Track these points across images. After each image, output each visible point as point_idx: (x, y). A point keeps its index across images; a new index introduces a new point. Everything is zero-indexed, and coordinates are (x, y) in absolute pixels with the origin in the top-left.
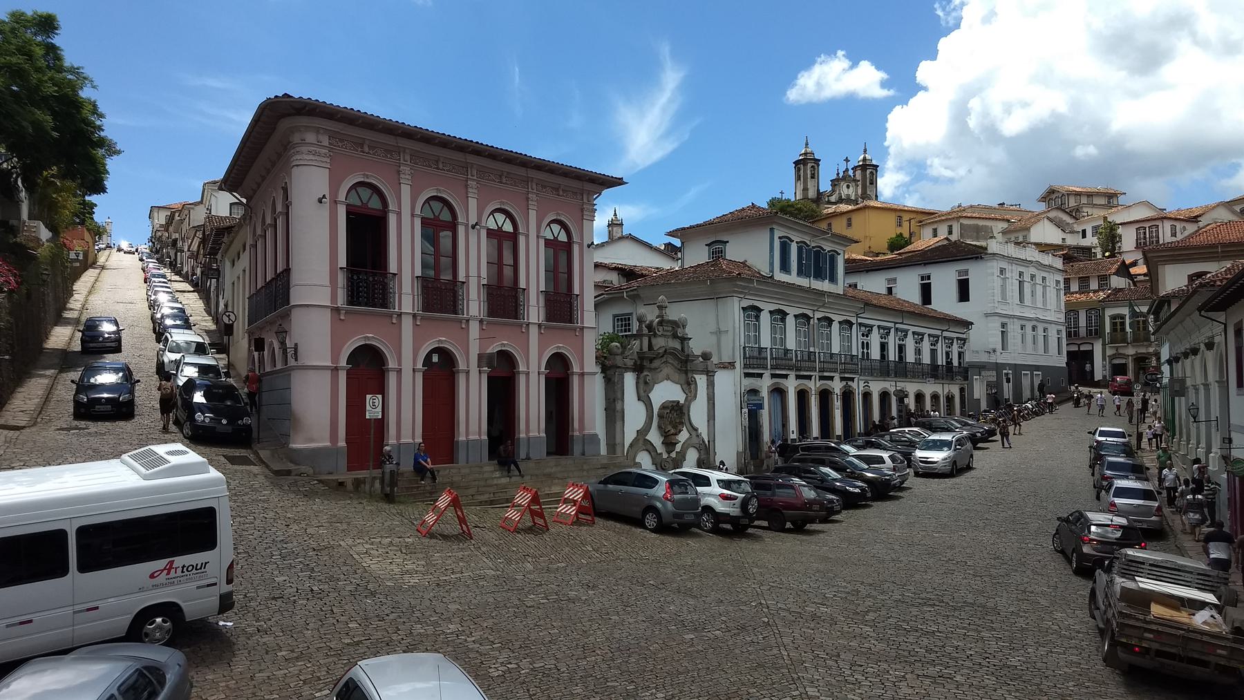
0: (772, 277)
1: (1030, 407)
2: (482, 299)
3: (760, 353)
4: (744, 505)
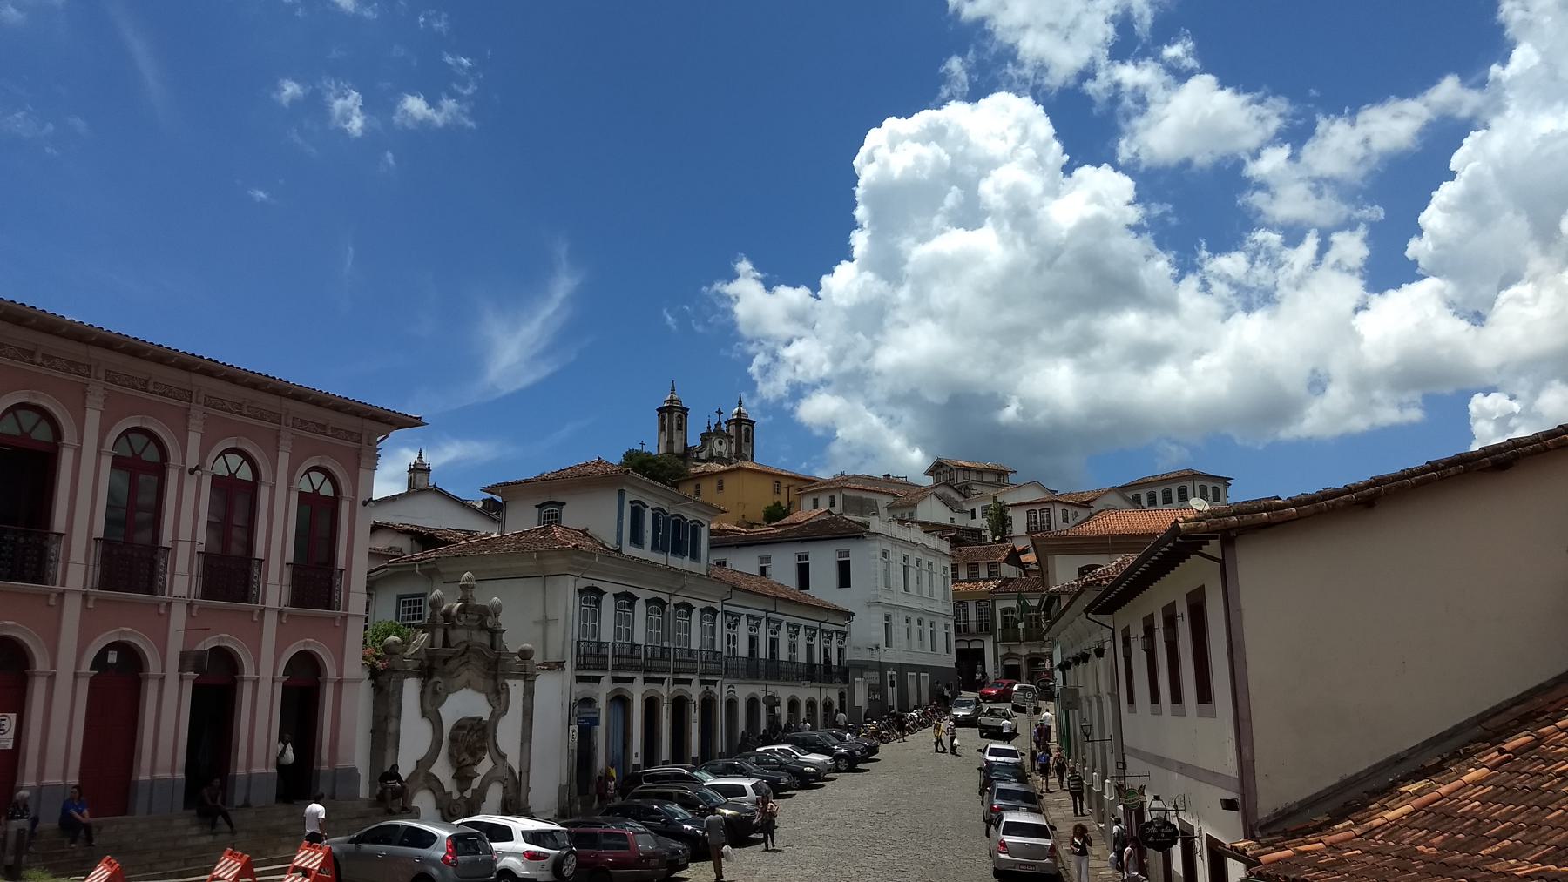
0: (619, 551)
2: (194, 573)
3: (598, 650)
4: (558, 865)
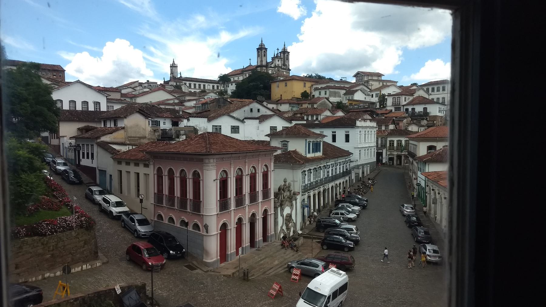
1: (370, 183)
